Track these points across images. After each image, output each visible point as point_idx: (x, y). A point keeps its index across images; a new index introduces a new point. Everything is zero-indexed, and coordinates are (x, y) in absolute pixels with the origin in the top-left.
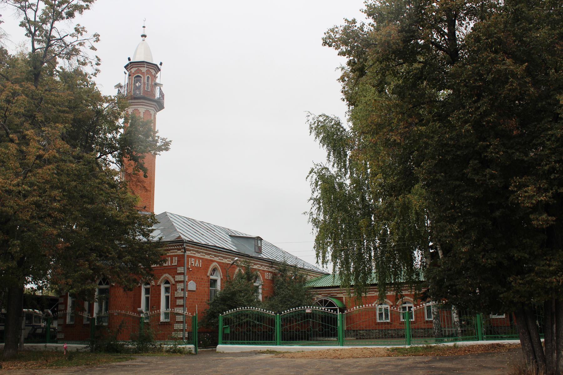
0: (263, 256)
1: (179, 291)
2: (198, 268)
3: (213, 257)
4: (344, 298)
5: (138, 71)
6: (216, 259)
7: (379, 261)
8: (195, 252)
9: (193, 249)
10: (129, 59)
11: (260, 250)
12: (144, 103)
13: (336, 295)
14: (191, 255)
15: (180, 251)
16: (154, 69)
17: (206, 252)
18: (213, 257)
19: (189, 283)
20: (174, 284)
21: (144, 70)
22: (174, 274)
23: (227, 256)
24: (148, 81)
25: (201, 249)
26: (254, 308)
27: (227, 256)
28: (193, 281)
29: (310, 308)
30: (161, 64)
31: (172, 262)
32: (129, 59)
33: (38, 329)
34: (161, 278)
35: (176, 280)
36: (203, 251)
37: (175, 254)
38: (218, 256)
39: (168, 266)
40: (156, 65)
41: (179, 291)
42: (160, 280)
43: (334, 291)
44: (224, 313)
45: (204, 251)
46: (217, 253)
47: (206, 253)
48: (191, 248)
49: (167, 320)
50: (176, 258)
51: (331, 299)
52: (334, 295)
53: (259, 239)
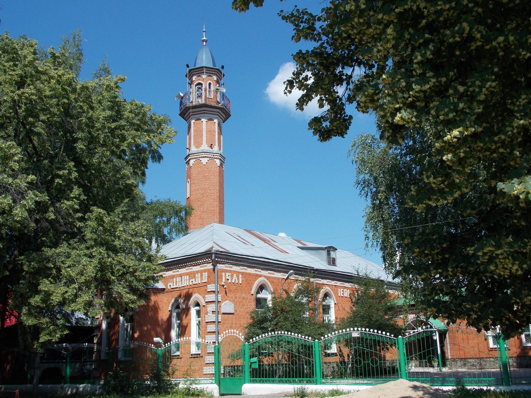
0: (339, 268)
7: (398, 186)
10: (188, 66)
16: (216, 74)
19: (222, 304)
20: (204, 306)
22: (204, 294)
24: (210, 88)
29: (358, 330)
30: (223, 67)
32: (188, 66)
41: (210, 314)
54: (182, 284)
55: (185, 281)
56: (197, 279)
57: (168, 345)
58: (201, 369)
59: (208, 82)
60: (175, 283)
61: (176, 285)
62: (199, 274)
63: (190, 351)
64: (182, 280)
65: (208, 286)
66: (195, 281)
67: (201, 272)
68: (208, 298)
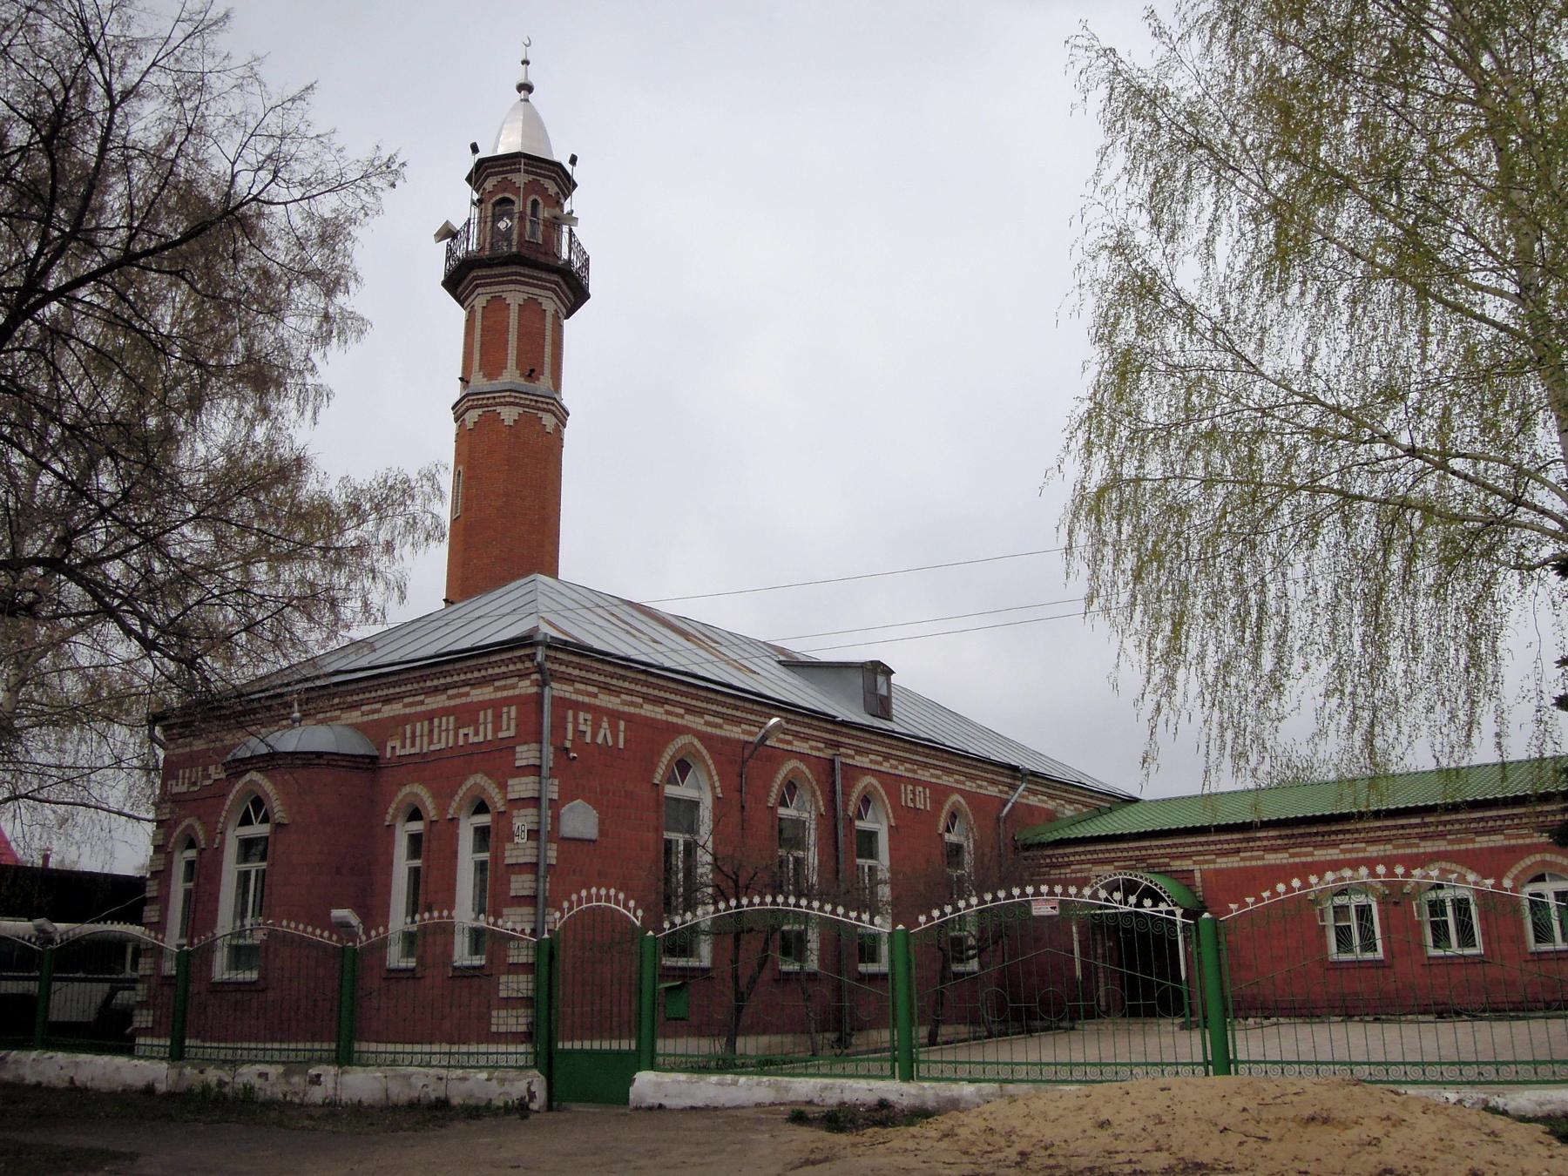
1: (521, 840)
2: (608, 753)
3: (677, 715)
4: (1197, 875)
5: (507, 185)
6: (691, 721)
8: (595, 690)
9: (583, 674)
10: (475, 149)
11: (882, 706)
12: (520, 274)
13: (1167, 865)
14: (574, 697)
15: (527, 683)
16: (554, 179)
17: (645, 690)
18: (677, 715)
21: (520, 179)
23: (739, 714)
25: (624, 678)
26: (780, 899)
27: (739, 714)
28: (588, 801)
29: (1051, 893)
30: (573, 160)
31: (497, 728)
32: (475, 149)
33: (119, 995)
34: (461, 793)
35: (511, 796)
36: (632, 686)
37: (510, 693)
38: (700, 713)
39: (486, 742)
40: (559, 165)
42: (457, 798)
43: (1158, 847)
44: (285, 923)
45: (638, 688)
46: (697, 698)
47: (646, 698)
48: (576, 672)
49: (478, 961)
50: (513, 709)
51: (1148, 876)
52: (1159, 865)
53: (878, 670)
54: (431, 742)
55: (444, 734)
56: (482, 728)
57: (378, 934)
58: (486, 1019)
59: (532, 198)
60: (408, 742)
61: (413, 745)
62: (490, 712)
63: (451, 956)
64: (431, 731)
65: (518, 749)
66: (477, 733)
67: (497, 705)
68: (516, 788)
